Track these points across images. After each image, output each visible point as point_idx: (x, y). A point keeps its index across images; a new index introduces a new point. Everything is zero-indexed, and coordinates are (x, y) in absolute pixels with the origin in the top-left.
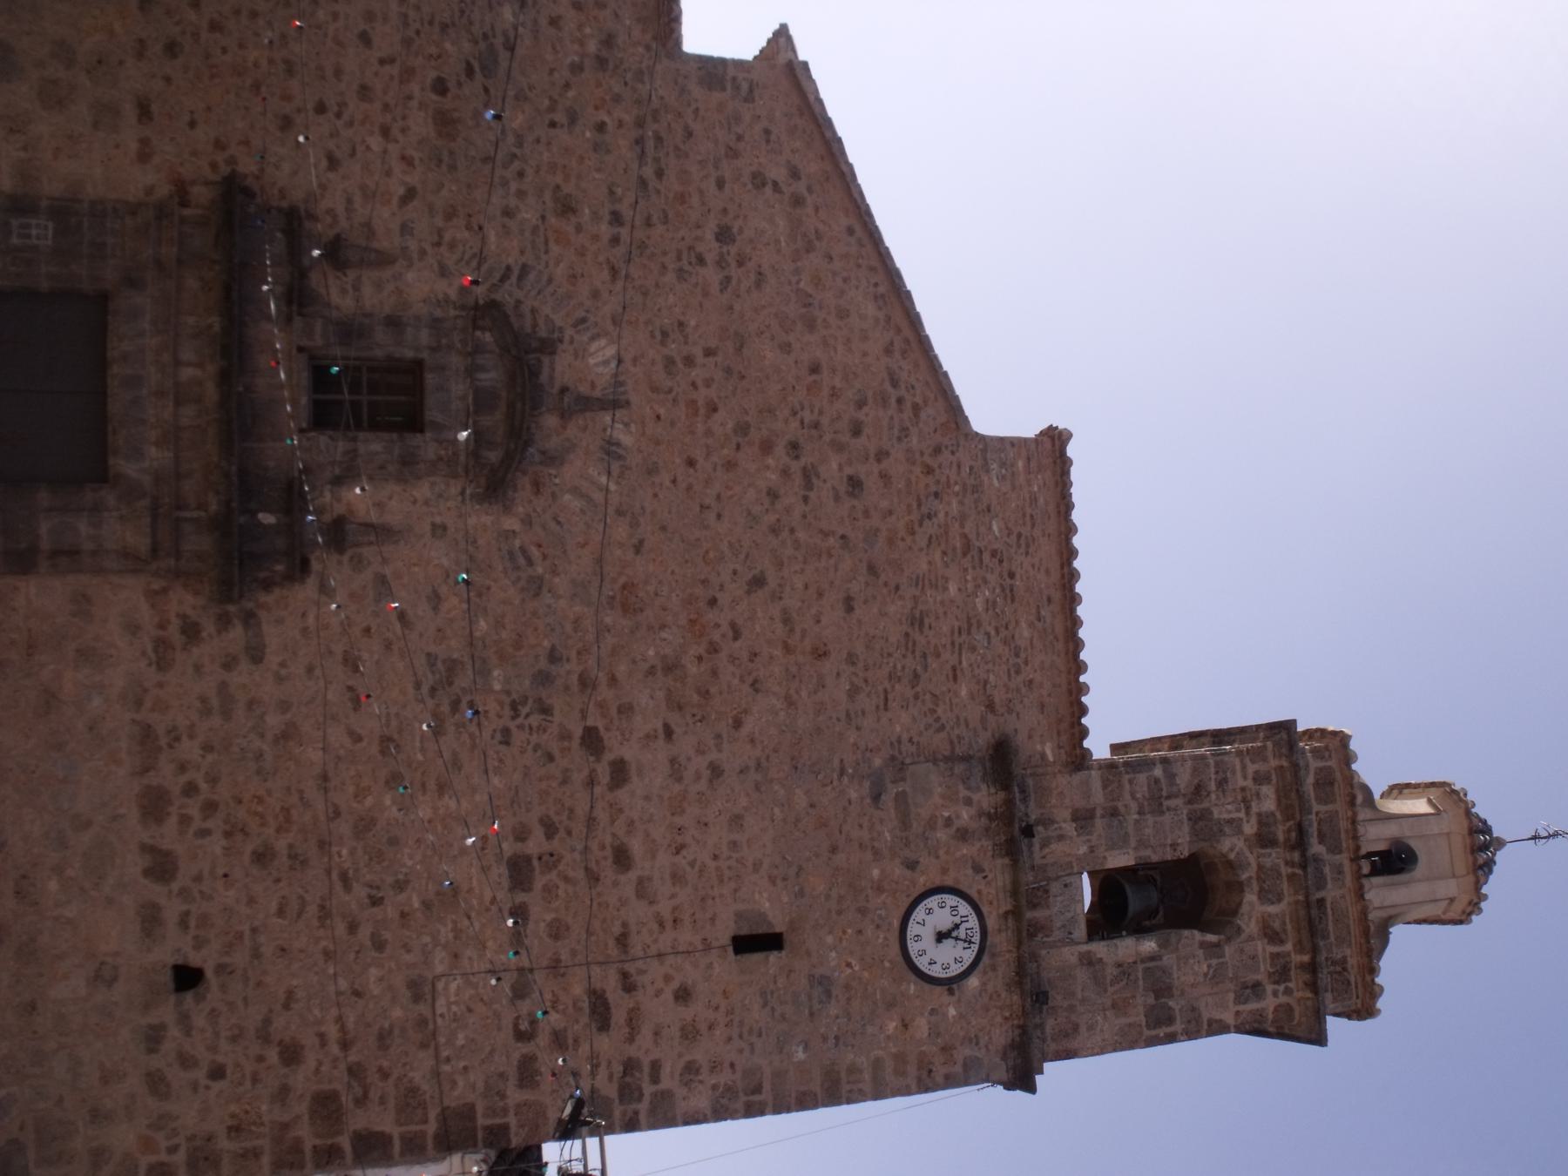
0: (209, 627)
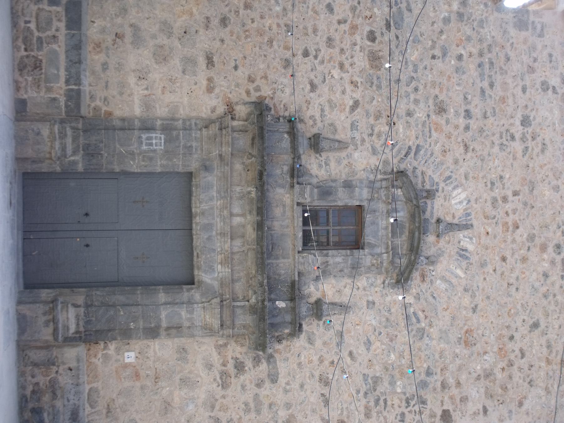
0: (249, 364)
